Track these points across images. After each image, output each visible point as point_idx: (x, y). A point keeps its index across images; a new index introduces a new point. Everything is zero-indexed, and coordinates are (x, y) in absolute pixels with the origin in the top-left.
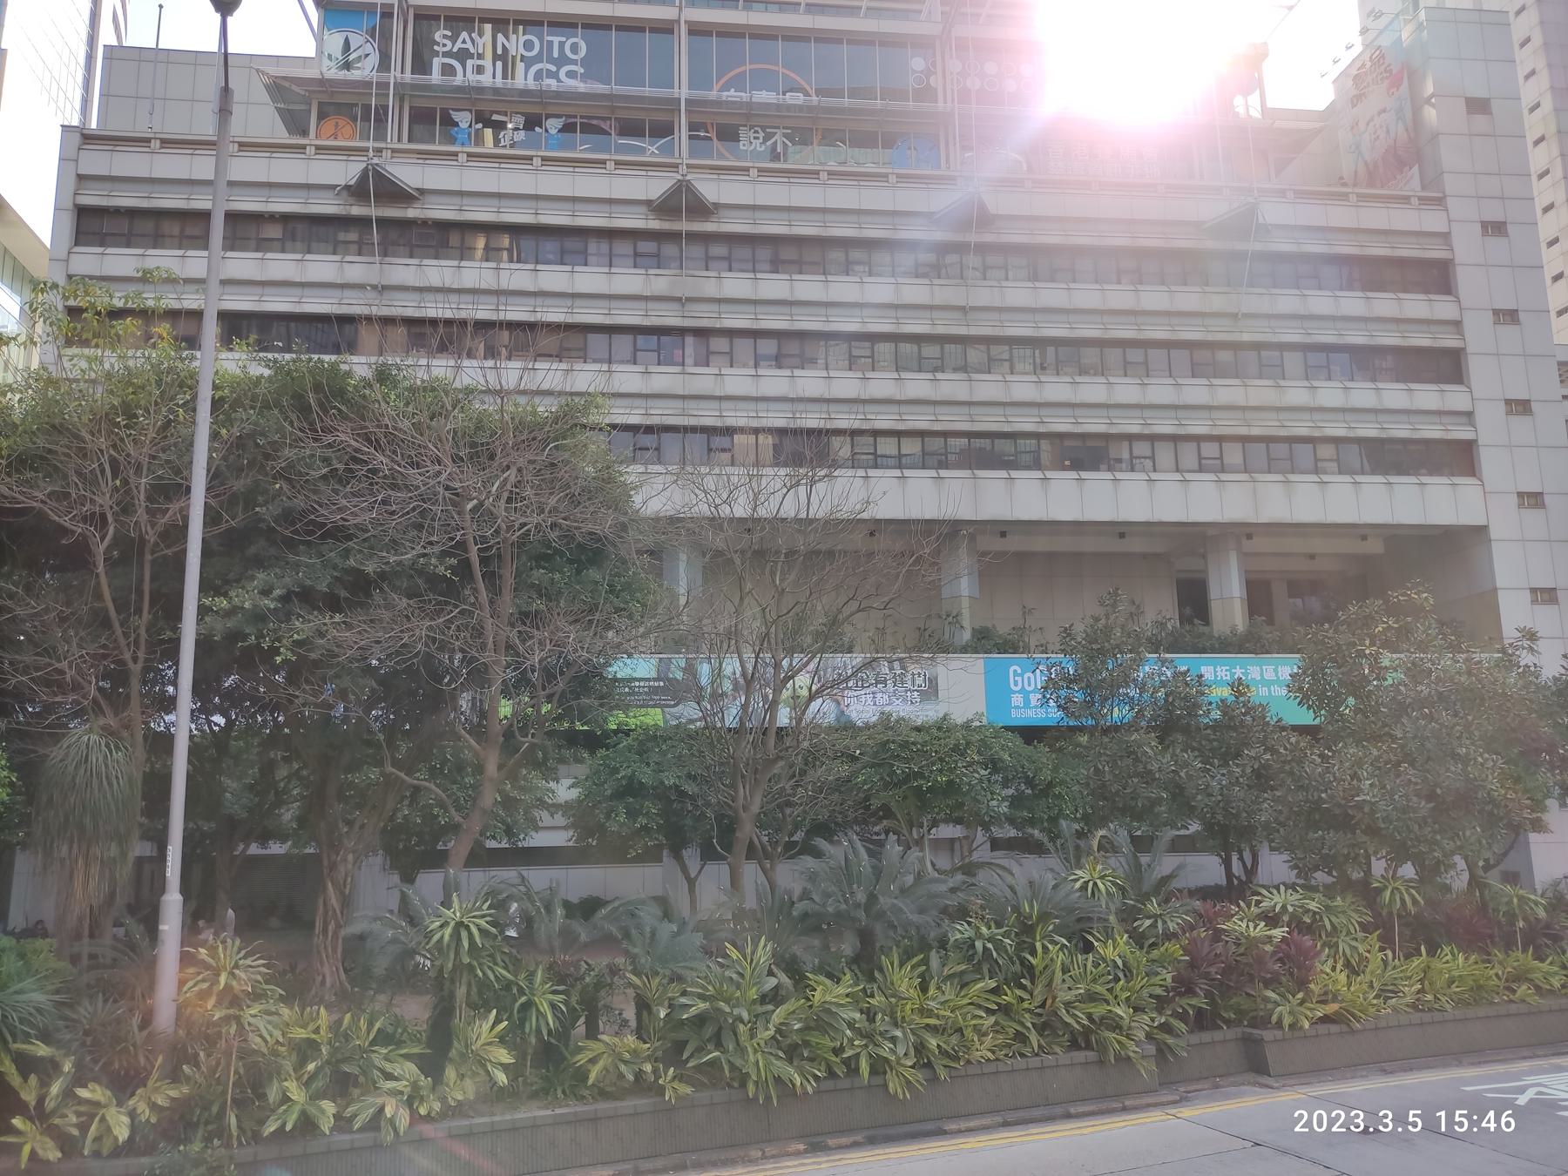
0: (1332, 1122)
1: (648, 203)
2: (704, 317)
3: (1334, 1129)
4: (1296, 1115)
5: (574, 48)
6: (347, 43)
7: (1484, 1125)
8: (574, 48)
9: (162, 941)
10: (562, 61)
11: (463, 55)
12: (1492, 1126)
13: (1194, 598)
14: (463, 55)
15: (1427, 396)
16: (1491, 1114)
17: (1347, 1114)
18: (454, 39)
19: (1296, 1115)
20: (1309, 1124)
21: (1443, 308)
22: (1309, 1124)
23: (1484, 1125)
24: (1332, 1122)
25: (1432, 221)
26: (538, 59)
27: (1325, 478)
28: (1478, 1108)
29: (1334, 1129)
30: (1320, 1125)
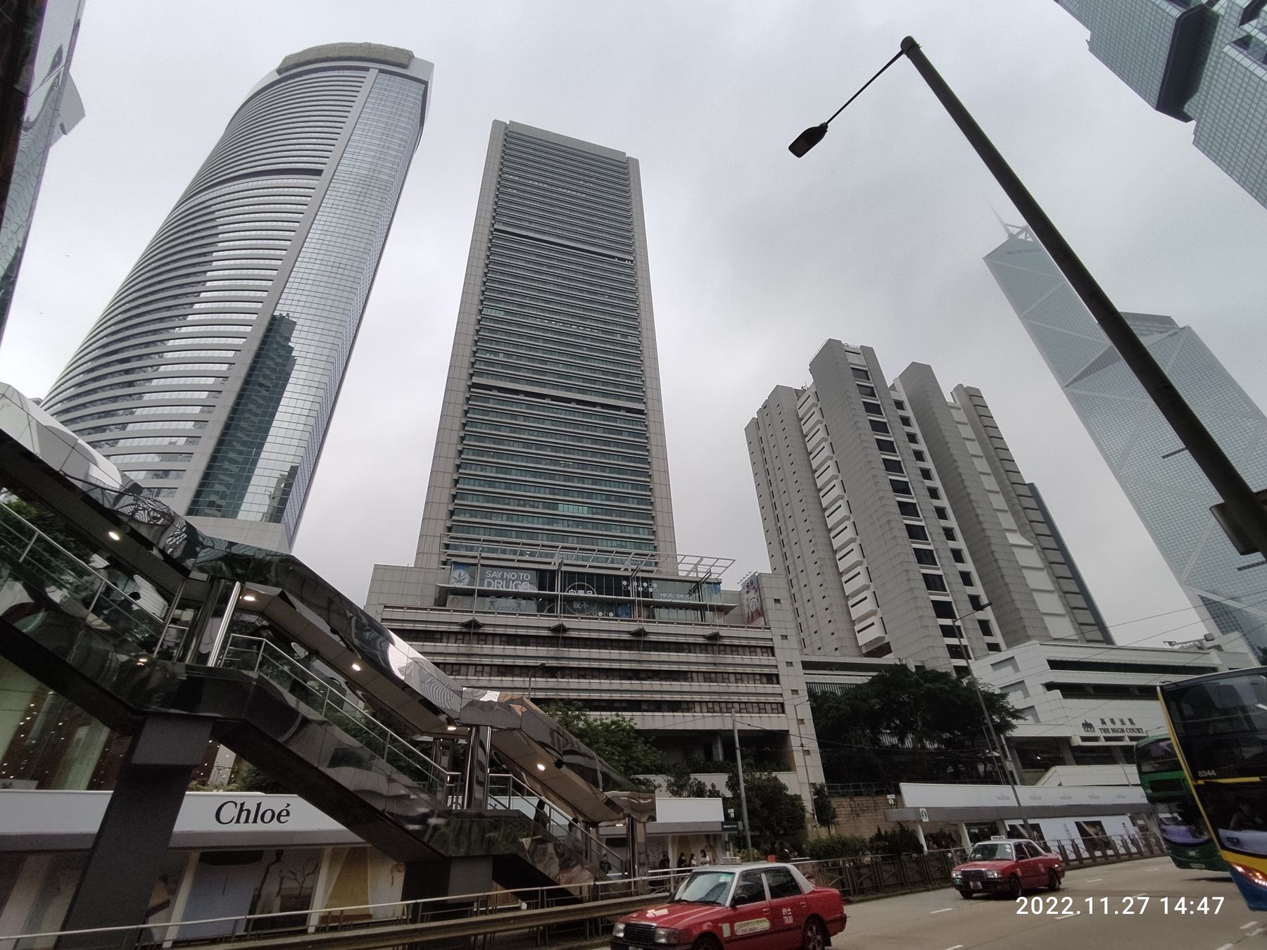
0: (1047, 906)
1: (549, 628)
2: (564, 663)
3: (1049, 912)
4: (1124, 901)
5: (527, 577)
6: (460, 574)
7: (1199, 908)
8: (527, 577)
9: (61, 86)
10: (523, 581)
11: (494, 579)
12: (1183, 910)
13: (709, 754)
14: (494, 579)
15: (769, 688)
16: (1183, 900)
17: (1059, 901)
18: (492, 574)
19: (1124, 901)
20: (1028, 908)
21: (771, 660)
22: (1028, 908)
23: (1199, 908)
24: (1047, 906)
25: (767, 635)
26: (516, 580)
27: (743, 715)
28: (1116, 895)
29: (1049, 912)
30: (1037, 909)
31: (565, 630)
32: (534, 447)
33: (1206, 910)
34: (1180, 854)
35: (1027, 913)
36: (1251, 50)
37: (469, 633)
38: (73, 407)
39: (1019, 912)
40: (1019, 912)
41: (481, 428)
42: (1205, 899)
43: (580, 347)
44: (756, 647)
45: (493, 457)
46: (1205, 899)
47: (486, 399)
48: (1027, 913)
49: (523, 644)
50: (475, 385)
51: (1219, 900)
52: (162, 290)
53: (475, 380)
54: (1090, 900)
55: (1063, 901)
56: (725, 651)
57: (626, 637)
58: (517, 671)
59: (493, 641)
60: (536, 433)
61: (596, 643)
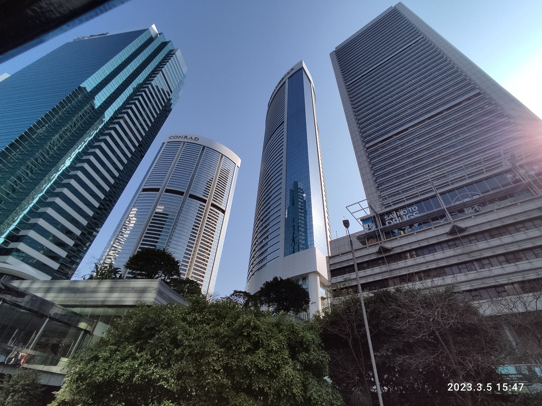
0: (461, 387)
3: (462, 390)
4: (448, 385)
19: (448, 385)
23: (513, 388)
24: (461, 387)
29: (462, 390)
32: (414, 155)
33: (516, 389)
35: (452, 390)
36: (92, 368)
38: (265, 211)
39: (449, 390)
40: (449, 390)
41: (380, 164)
42: (516, 384)
43: (416, 94)
44: (472, 261)
45: (393, 173)
46: (516, 384)
47: (377, 150)
48: (452, 390)
50: (368, 148)
51: (521, 385)
52: (274, 148)
53: (367, 146)
54: (499, 384)
55: (461, 385)
60: (415, 147)
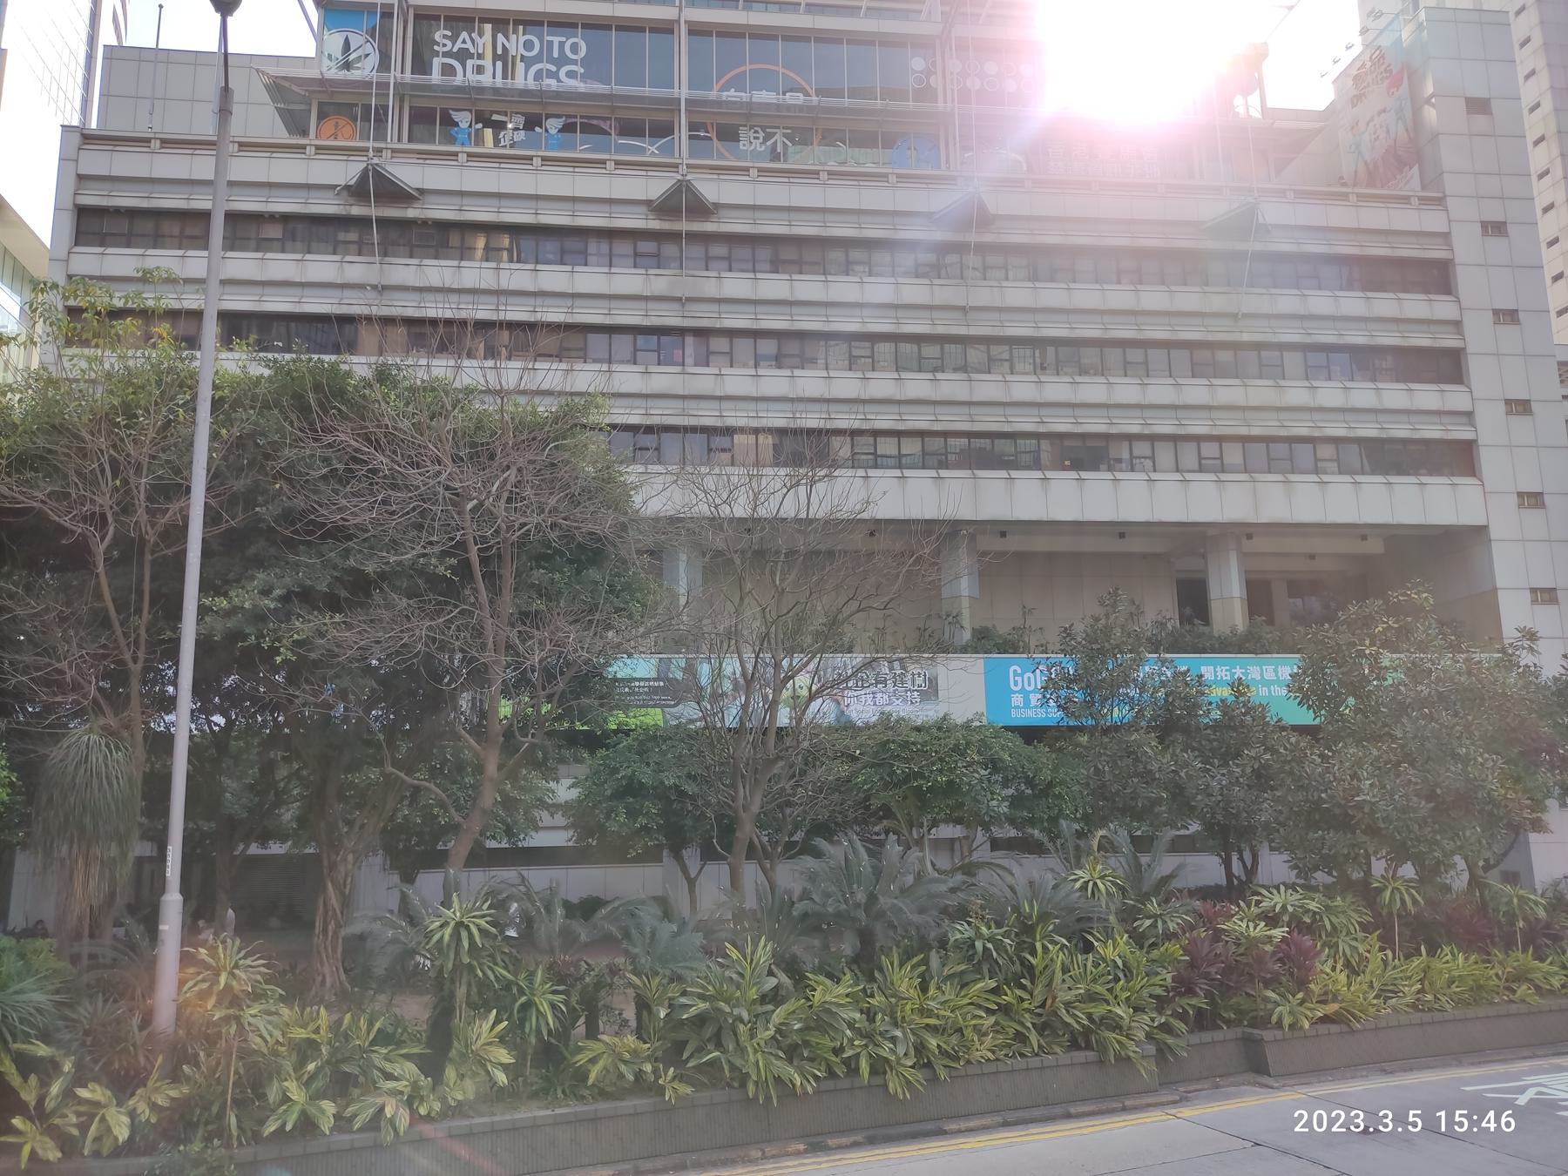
0: (1332, 1122)
1: (648, 203)
3: (1334, 1129)
4: (1296, 1115)
5: (574, 48)
6: (347, 43)
8: (574, 48)
10: (562, 61)
13: (1194, 598)
14: (463, 55)
15: (1427, 396)
16: (1491, 1114)
18: (454, 39)
19: (1296, 1115)
20: (1309, 1124)
21: (1443, 308)
22: (1309, 1124)
24: (1332, 1122)
25: (1432, 221)
26: (538, 59)
27: (1325, 478)
29: (1334, 1129)
30: (1320, 1125)
31: (701, 209)
34: (1484, 961)
37: (674, 236)
49: (776, 266)
56: (728, 259)
57: (326, 206)
58: (547, 342)
59: (470, 248)
61: (123, 225)
